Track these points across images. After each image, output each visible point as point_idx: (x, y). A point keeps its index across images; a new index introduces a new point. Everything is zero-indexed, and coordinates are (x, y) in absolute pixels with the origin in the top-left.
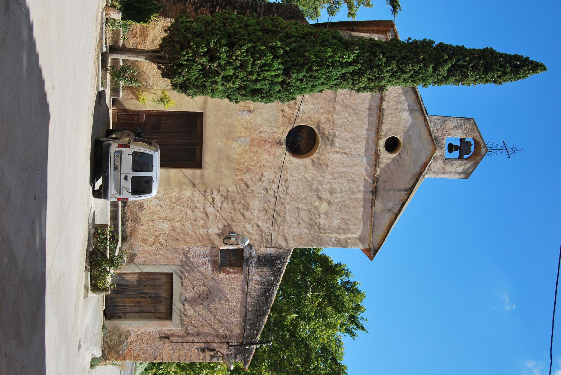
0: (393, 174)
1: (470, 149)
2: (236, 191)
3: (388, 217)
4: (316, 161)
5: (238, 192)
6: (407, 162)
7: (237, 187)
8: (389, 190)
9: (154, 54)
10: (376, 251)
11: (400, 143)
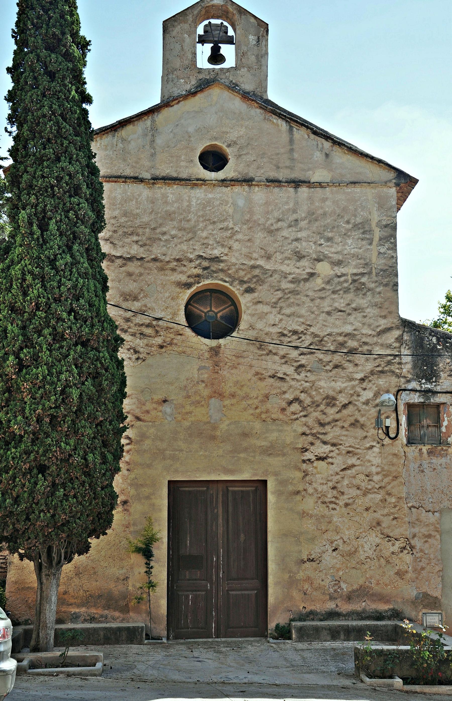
0: (264, 154)
1: (216, 25)
2: (303, 419)
3: (340, 157)
4: (245, 286)
5: (305, 416)
6: (243, 131)
7: (297, 419)
8: (292, 159)
9: (44, 570)
10: (400, 174)
11: (211, 146)
